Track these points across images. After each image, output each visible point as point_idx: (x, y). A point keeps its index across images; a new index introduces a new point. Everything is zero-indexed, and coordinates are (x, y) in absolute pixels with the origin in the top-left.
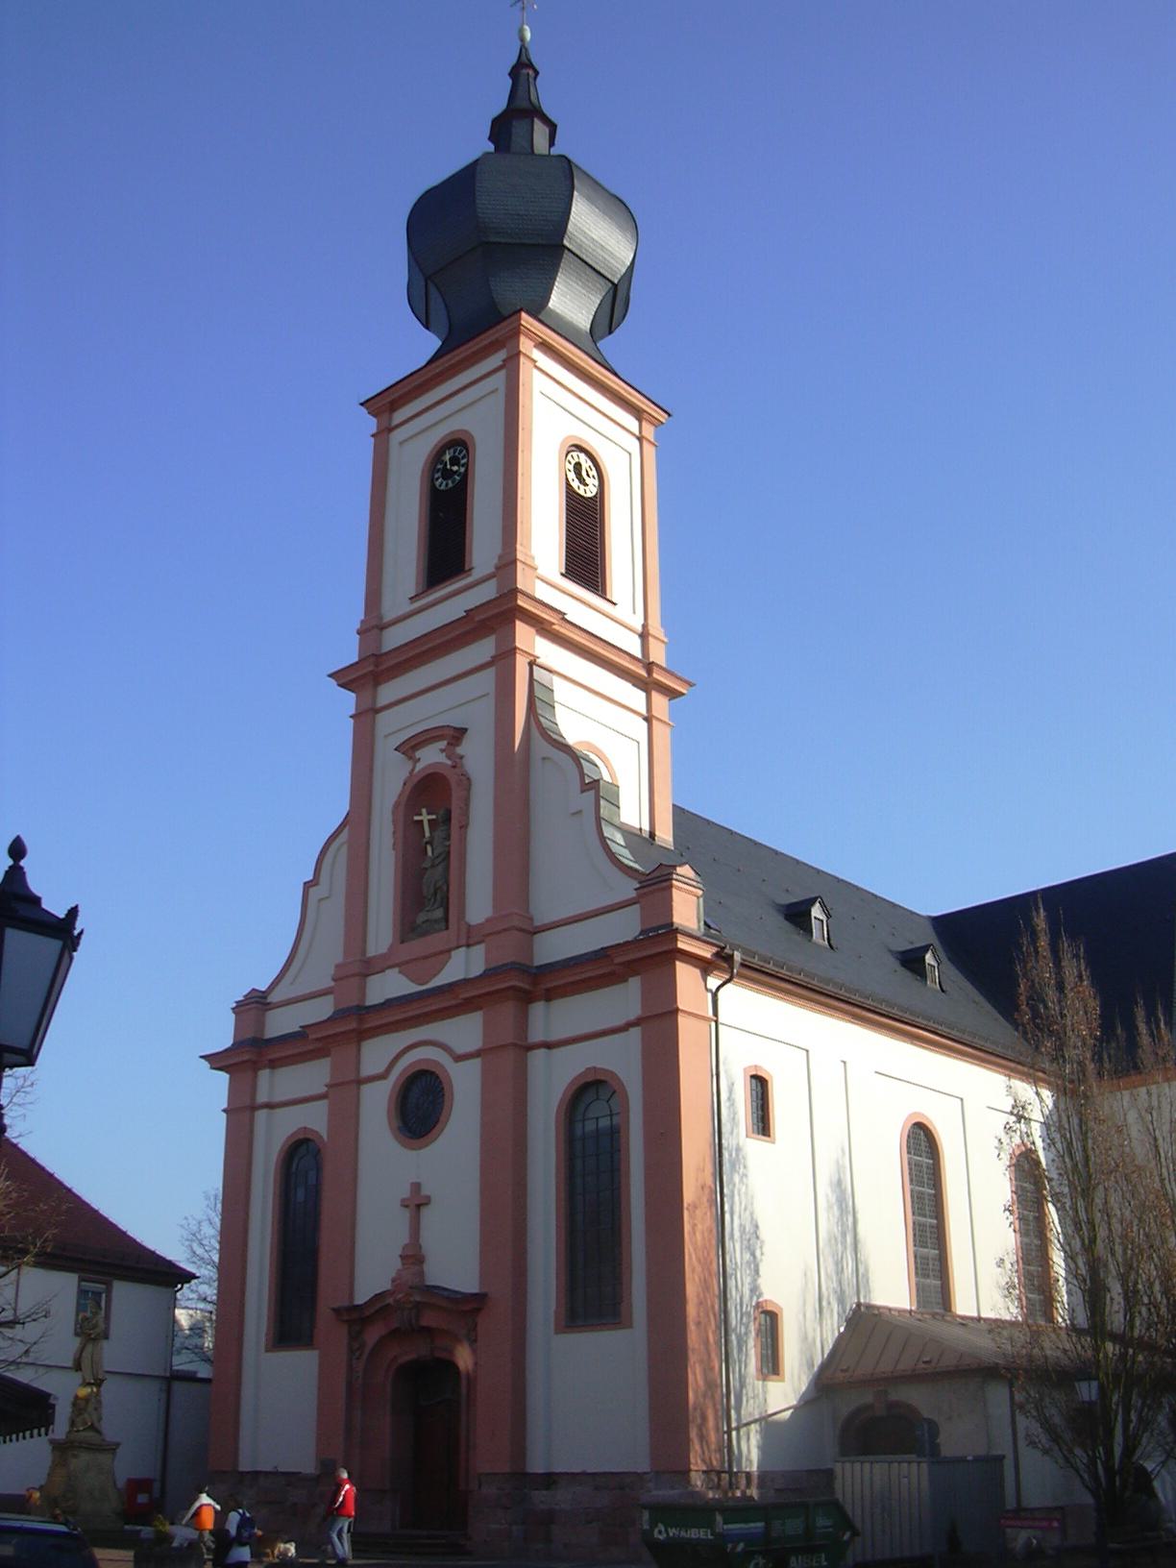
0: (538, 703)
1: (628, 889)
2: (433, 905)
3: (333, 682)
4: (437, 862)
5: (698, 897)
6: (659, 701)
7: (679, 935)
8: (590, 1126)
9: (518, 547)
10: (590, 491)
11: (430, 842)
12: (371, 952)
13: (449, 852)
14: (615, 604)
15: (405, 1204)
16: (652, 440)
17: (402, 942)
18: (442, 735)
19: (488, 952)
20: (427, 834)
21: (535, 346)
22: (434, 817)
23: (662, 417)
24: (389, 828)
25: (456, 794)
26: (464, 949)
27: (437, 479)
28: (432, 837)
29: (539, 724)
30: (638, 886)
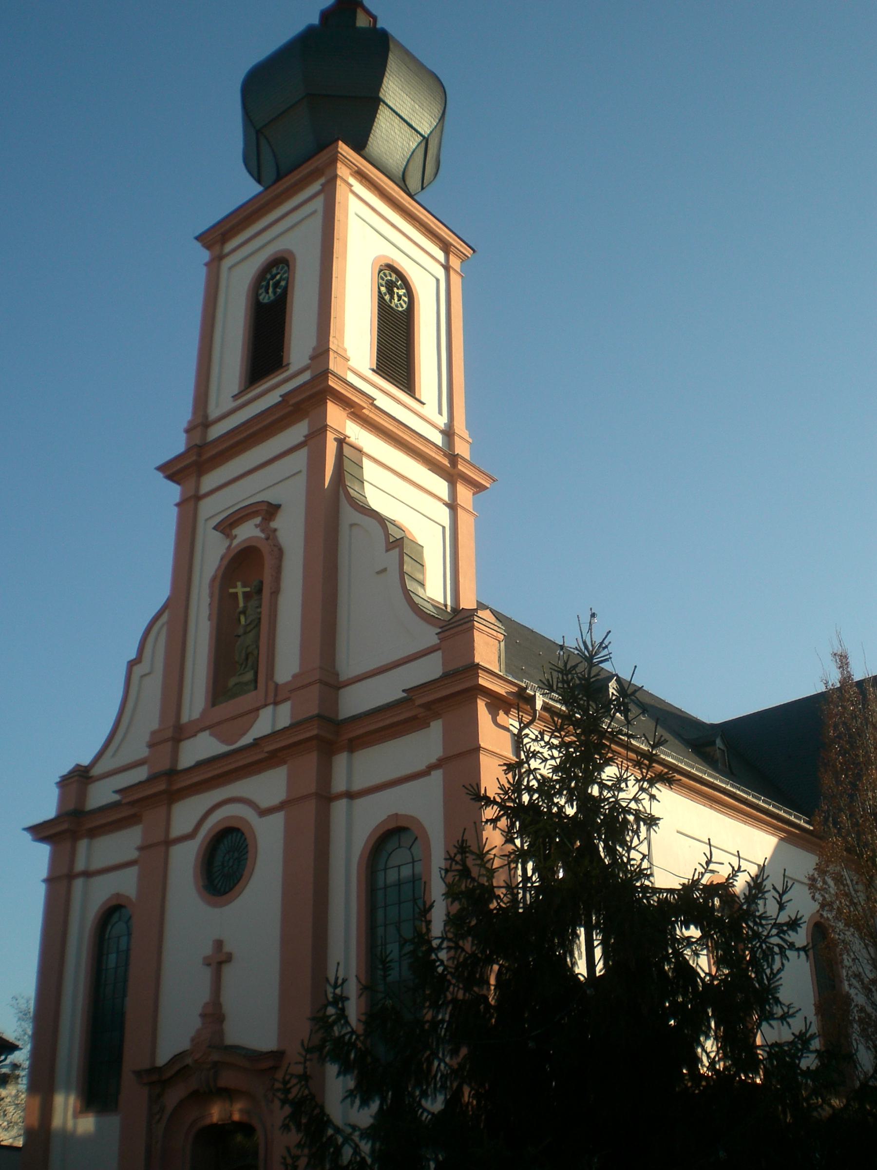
0: (346, 461)
1: (430, 636)
2: (245, 667)
3: (160, 475)
4: (249, 629)
5: (499, 642)
6: (464, 494)
7: (480, 671)
8: (392, 876)
9: (331, 339)
10: (399, 304)
11: (244, 612)
12: (185, 719)
13: (260, 619)
14: (424, 404)
15: (207, 962)
16: (459, 271)
17: (214, 704)
18: (257, 511)
19: (292, 708)
20: (241, 604)
21: (351, 174)
22: (248, 589)
23: (468, 252)
24: (205, 600)
25: (269, 562)
26: (270, 708)
27: (261, 294)
28: (245, 607)
29: (347, 494)
30: (439, 630)
